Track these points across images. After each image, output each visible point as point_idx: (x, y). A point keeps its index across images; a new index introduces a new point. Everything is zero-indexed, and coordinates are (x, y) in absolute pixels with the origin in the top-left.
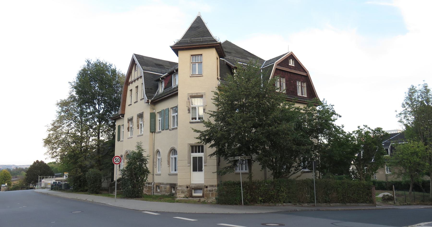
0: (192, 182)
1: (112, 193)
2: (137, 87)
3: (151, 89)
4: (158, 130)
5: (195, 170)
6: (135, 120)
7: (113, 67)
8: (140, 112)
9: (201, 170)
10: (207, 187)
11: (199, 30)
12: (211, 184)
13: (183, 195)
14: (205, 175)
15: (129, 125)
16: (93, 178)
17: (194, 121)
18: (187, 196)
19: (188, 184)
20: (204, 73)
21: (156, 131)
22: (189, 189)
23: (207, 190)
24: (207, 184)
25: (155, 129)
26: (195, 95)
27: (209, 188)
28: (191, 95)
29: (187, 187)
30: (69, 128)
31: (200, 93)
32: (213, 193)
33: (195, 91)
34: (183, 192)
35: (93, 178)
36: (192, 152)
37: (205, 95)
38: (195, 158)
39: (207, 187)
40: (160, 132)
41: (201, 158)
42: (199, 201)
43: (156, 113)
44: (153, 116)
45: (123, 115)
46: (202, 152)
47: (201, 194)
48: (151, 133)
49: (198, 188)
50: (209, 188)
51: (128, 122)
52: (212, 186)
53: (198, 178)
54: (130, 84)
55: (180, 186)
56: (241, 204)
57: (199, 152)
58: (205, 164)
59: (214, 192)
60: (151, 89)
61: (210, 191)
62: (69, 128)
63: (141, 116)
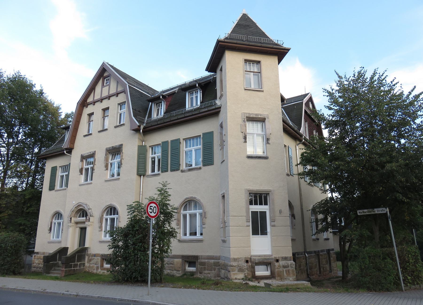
0: (253, 253)
1: (49, 273)
2: (105, 110)
3: (139, 111)
4: (57, 187)
5: (255, 232)
6: (100, 157)
7: (37, 88)
8: (116, 144)
9: (264, 232)
10: (277, 261)
11: (250, 29)
12: (284, 256)
13: (241, 276)
14: (272, 241)
15: (83, 165)
16: (11, 247)
17: (113, 178)
18: (250, 277)
19: (246, 255)
20: (265, 88)
21: (147, 174)
22: (250, 264)
23: (279, 266)
24: (277, 256)
25: (145, 171)
26: (254, 116)
27: (281, 263)
28: (247, 115)
29: (247, 262)
30: (218, 102)
31: (261, 115)
32: (289, 270)
33: (254, 111)
34: (241, 270)
35: (11, 247)
36: (251, 203)
37: (268, 118)
38: (254, 214)
39: (277, 261)
40: (159, 174)
41: (263, 214)
42: (268, 285)
43: (148, 146)
44: (142, 153)
45: (70, 151)
46: (266, 204)
47: (268, 273)
48: (138, 177)
49: (266, 262)
50: (281, 263)
51: (82, 161)
52: (285, 259)
53: (261, 246)
54: (89, 106)
55: (235, 260)
56: (144, 282)
57: (261, 204)
58: (273, 223)
59: (290, 268)
60: (139, 111)
61: (284, 267)
62: (218, 102)
63: (115, 151)
